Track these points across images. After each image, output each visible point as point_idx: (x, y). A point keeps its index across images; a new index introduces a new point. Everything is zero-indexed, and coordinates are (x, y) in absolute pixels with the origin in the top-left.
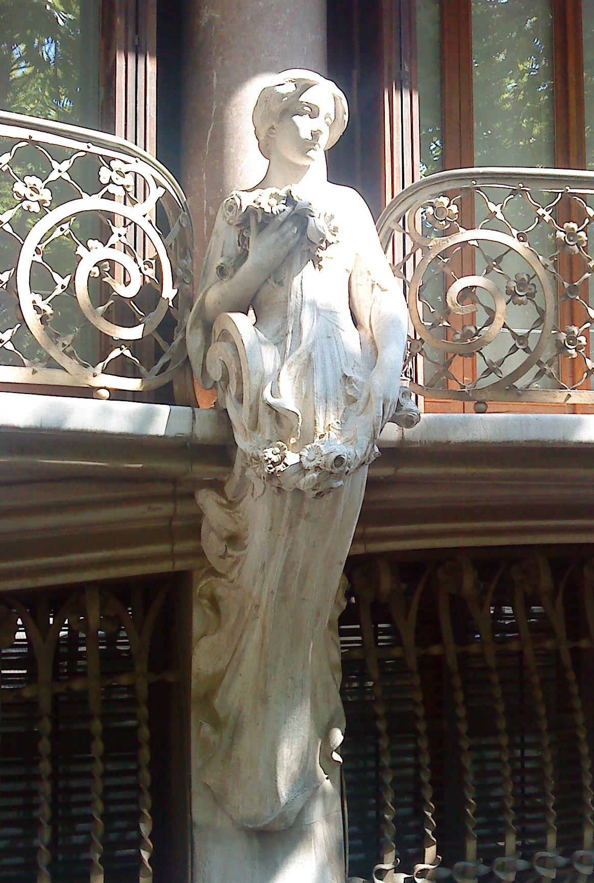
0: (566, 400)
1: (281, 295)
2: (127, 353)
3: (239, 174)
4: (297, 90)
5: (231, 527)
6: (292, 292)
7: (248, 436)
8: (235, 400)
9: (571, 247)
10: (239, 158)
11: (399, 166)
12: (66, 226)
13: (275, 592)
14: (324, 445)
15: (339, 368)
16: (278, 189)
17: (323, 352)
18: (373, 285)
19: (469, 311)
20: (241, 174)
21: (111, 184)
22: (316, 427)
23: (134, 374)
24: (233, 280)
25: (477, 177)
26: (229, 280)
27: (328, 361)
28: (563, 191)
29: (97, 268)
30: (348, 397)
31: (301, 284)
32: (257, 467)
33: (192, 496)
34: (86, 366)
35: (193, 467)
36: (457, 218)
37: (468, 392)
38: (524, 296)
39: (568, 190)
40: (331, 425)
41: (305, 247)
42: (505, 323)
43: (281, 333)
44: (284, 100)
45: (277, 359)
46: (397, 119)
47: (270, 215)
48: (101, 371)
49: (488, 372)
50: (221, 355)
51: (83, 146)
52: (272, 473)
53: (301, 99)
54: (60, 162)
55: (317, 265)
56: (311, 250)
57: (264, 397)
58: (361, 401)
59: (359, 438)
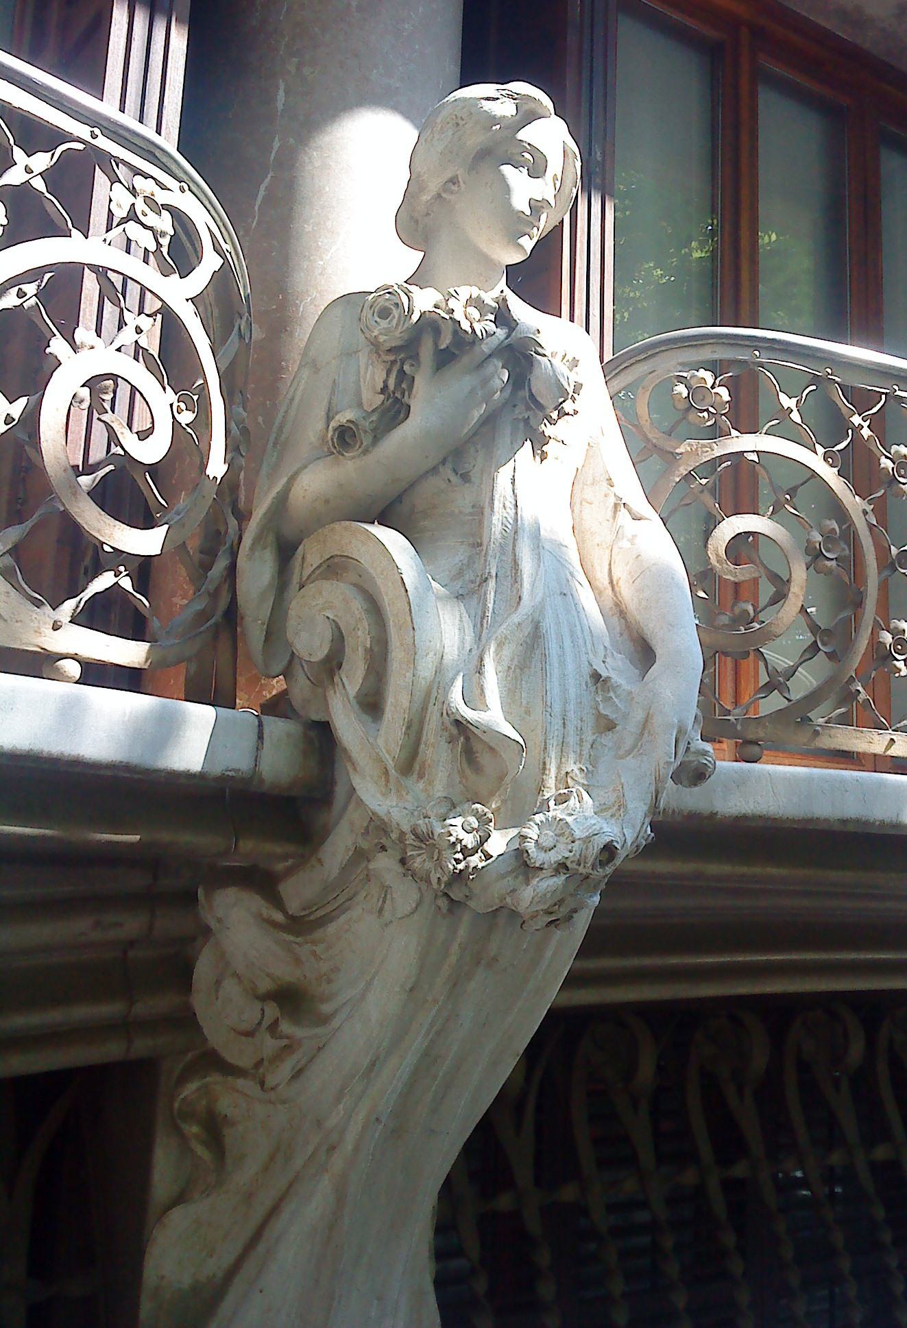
0: (888, 747)
1: (463, 500)
2: (126, 583)
3: (318, 272)
4: (517, 117)
5: (285, 972)
6: (497, 497)
7: (391, 786)
8: (356, 707)
9: (901, 485)
10: (320, 243)
11: (581, 315)
12: (30, 289)
13: (383, 1119)
14: (574, 817)
15: (584, 658)
16: (482, 291)
17: (558, 624)
18: (616, 505)
19: (747, 577)
20: (321, 274)
21: (131, 222)
22: (544, 777)
23: (134, 628)
24: (371, 458)
25: (761, 344)
26: (359, 455)
27: (567, 643)
28: (888, 391)
29: (87, 390)
30: (599, 716)
31: (513, 483)
32: (419, 855)
33: (189, 899)
34: (38, 604)
35: (241, 843)
36: (727, 410)
37: (735, 721)
38: (832, 559)
39: (896, 391)
40: (570, 775)
41: (521, 413)
42: (802, 605)
43: (469, 576)
44: (494, 128)
45: (466, 627)
46: (582, 234)
47: (469, 338)
48: (69, 619)
49: (770, 687)
50: (331, 608)
51: (83, 131)
52: (461, 871)
53: (521, 135)
54: (29, 154)
55: (539, 452)
56: (532, 422)
57: (452, 705)
58: (627, 731)
59: (631, 806)
